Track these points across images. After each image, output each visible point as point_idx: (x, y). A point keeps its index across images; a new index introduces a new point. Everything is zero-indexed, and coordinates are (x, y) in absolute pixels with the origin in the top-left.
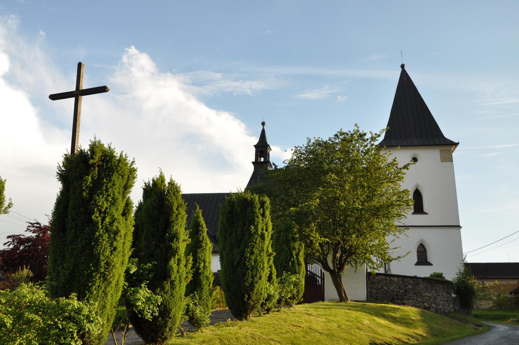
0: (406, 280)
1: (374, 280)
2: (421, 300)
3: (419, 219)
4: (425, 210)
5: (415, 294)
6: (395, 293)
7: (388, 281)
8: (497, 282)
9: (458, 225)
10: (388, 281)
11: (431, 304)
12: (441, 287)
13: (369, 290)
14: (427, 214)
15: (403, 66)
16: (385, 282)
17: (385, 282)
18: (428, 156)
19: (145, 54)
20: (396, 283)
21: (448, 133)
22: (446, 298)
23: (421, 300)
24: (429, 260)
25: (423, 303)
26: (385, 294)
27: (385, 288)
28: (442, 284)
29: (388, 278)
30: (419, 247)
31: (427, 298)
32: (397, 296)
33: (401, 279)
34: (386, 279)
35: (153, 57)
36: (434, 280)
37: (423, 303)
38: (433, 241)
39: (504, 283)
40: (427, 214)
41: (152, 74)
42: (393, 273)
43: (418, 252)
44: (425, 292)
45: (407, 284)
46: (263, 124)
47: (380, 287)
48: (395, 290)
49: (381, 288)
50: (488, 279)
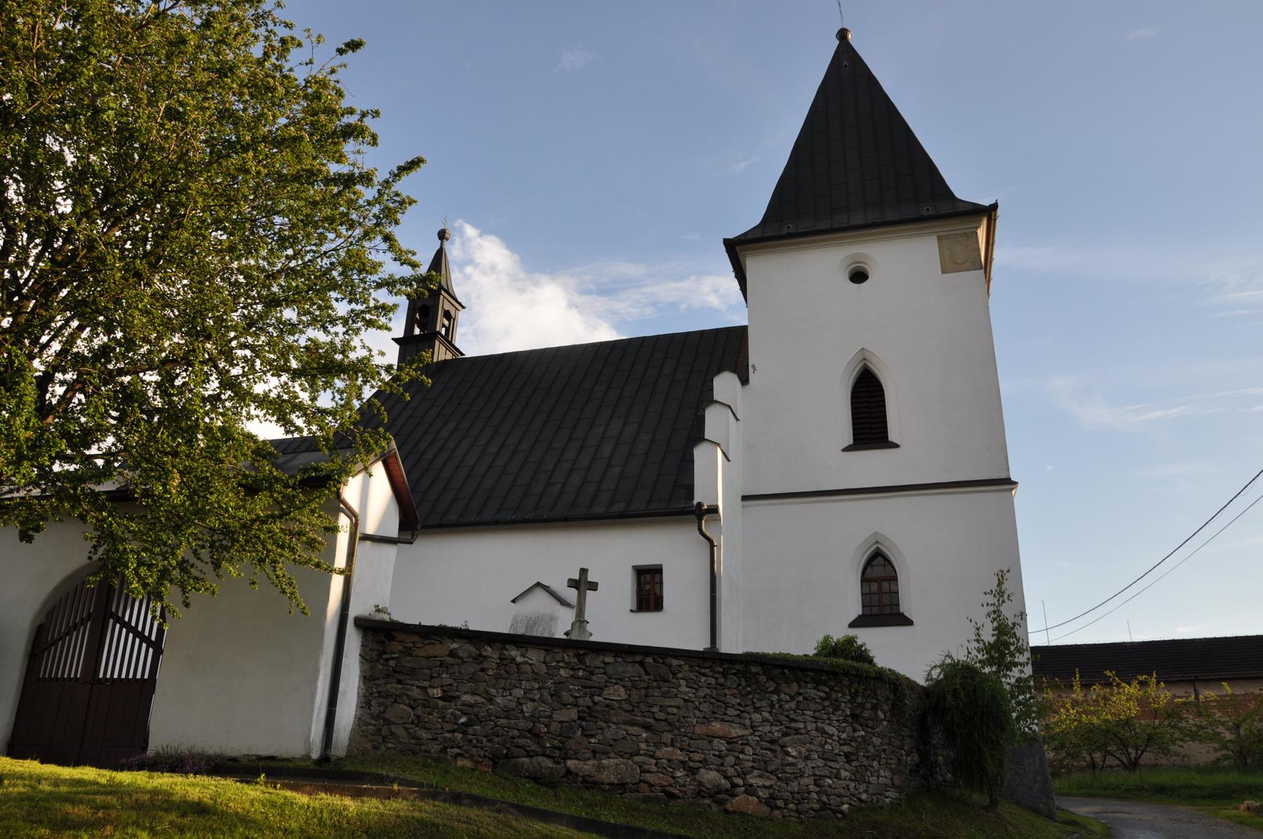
0: (595, 661)
1: (408, 662)
2: (679, 755)
3: (872, 467)
4: (893, 436)
5: (647, 727)
6: (522, 724)
7: (491, 666)
8: (1227, 689)
9: (1003, 476)
10: (491, 666)
11: (742, 775)
12: (813, 693)
13: (376, 709)
14: (897, 446)
15: (842, 34)
16: (471, 668)
17: (471, 668)
18: (904, 260)
19: (493, 238)
20: (536, 677)
21: (965, 185)
22: (842, 742)
23: (679, 755)
24: (906, 608)
25: (692, 771)
26: (463, 729)
27: (467, 698)
28: (817, 683)
29: (488, 651)
30: (869, 563)
31: (721, 745)
32: (536, 736)
33: (569, 656)
34: (480, 658)
35: (511, 241)
36: (820, 671)
37: (692, 771)
38: (926, 544)
39: (1257, 692)
40: (897, 446)
41: (514, 279)
42: (597, 637)
43: (865, 580)
44: (706, 720)
45: (599, 679)
46: (442, 235)
47: (437, 692)
48: (528, 708)
49: (447, 698)
50: (1211, 680)
